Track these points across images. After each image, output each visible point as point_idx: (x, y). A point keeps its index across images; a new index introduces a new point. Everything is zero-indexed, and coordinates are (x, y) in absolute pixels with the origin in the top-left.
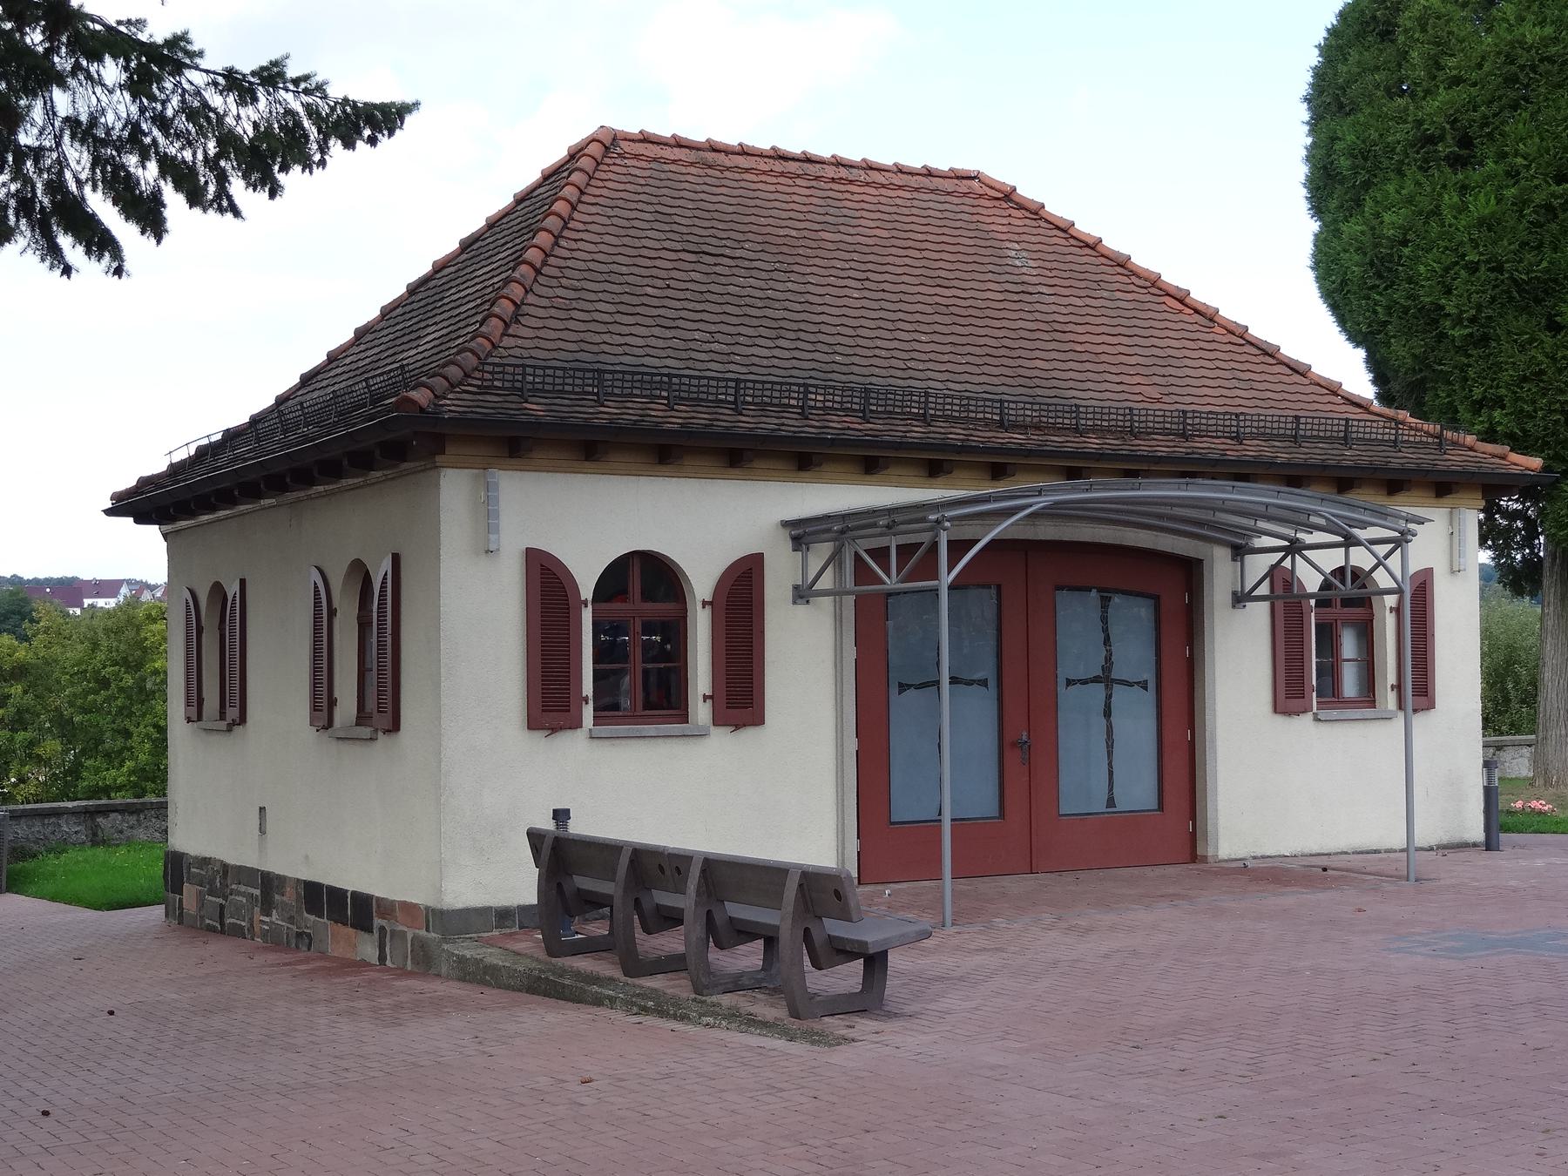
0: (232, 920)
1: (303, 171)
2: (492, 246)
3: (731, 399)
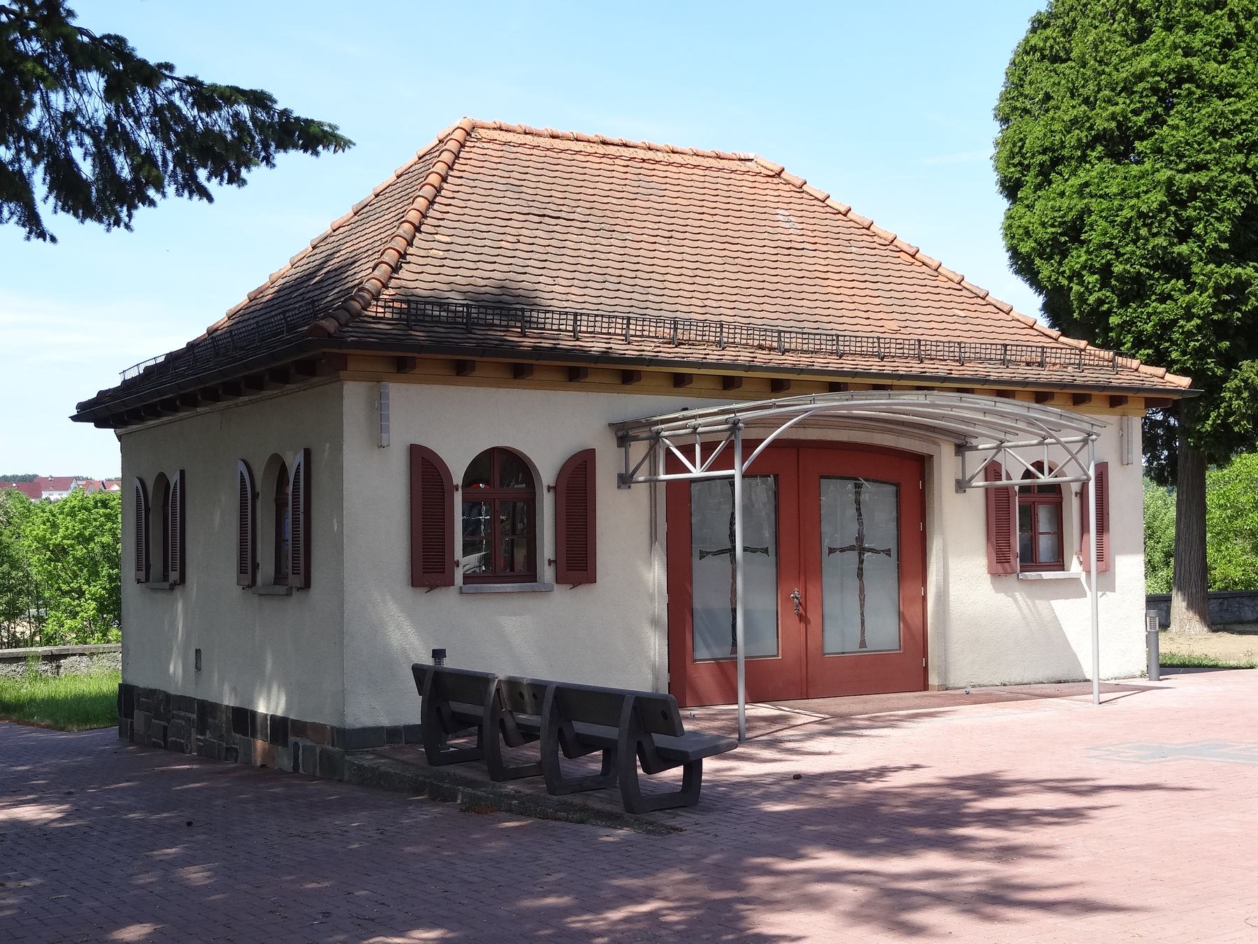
0: (173, 738)
1: (349, 147)
2: (378, 210)
3: (570, 328)
